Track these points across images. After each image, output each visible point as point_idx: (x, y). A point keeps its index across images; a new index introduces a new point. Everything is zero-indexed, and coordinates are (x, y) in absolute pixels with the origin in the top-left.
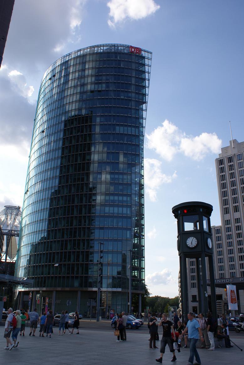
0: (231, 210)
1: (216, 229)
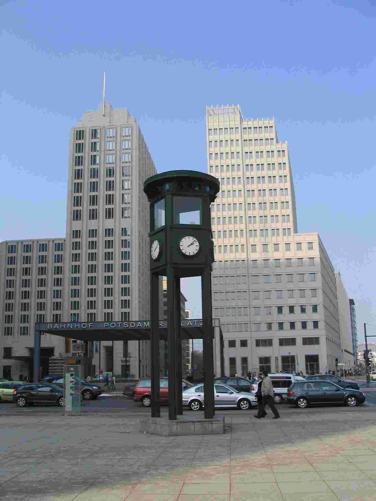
0: (85, 215)
1: (10, 244)
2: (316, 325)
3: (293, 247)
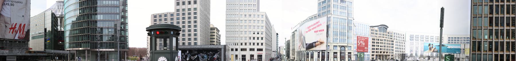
2: (262, 44)
3: (256, 16)
